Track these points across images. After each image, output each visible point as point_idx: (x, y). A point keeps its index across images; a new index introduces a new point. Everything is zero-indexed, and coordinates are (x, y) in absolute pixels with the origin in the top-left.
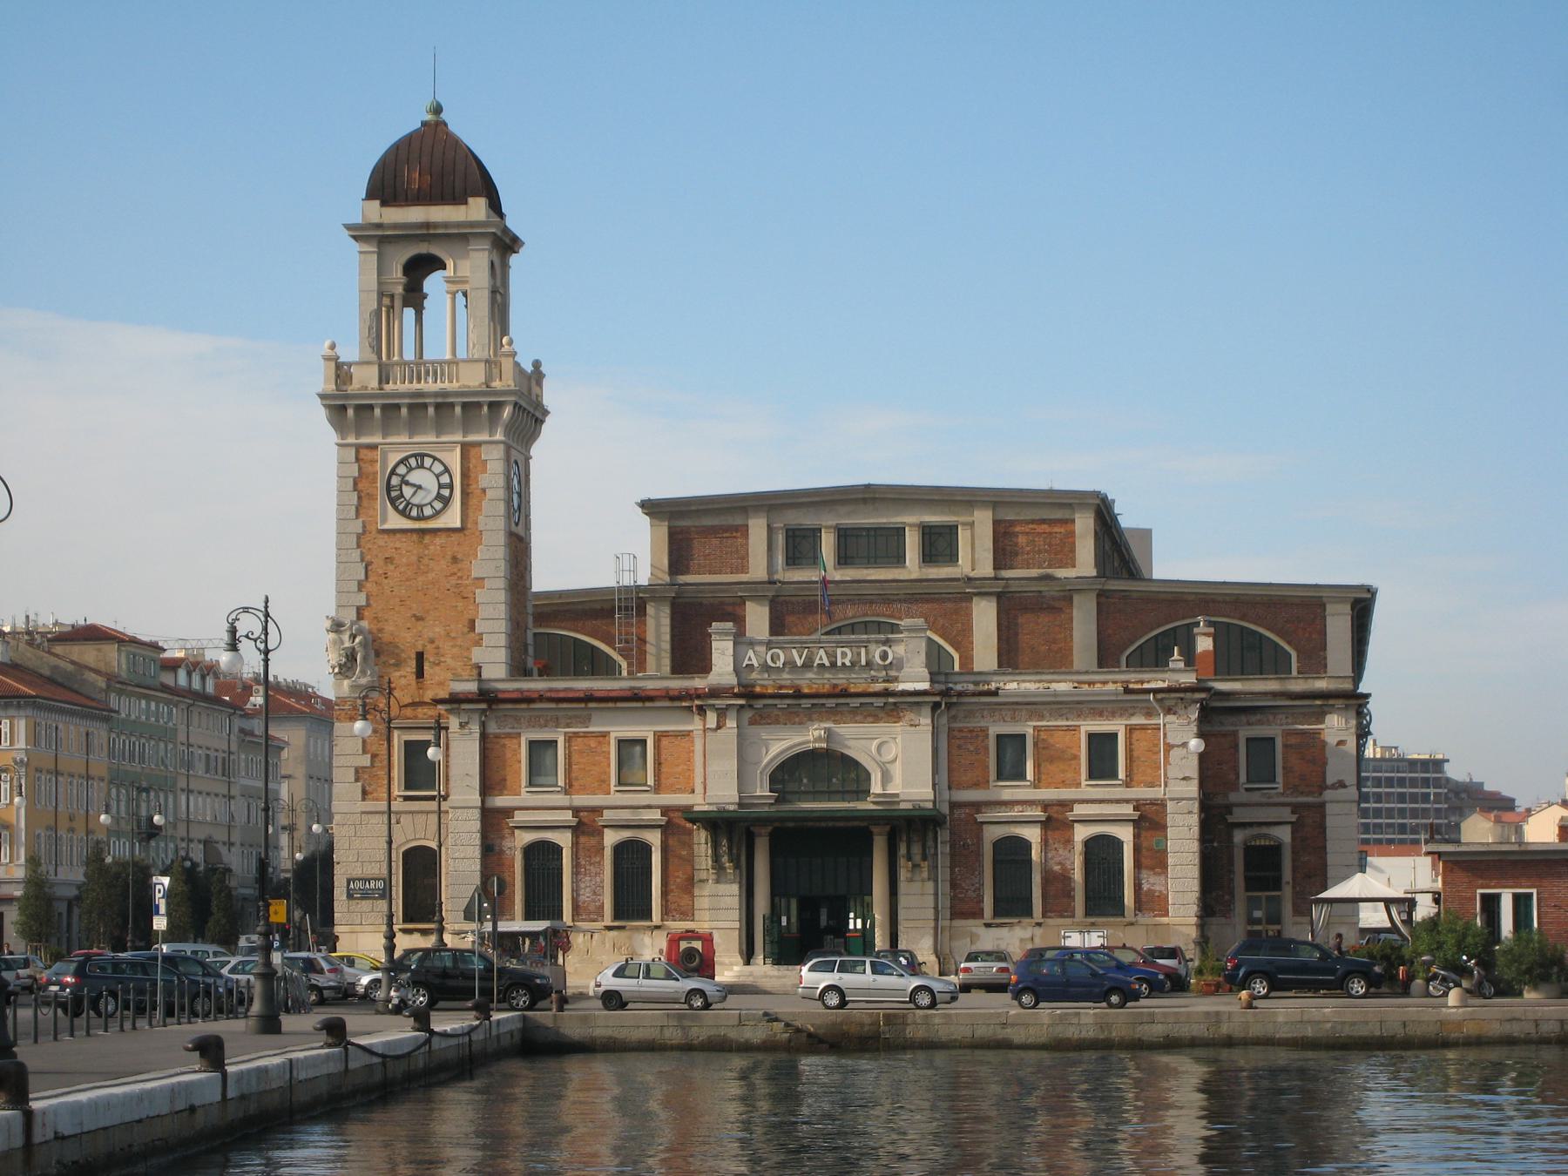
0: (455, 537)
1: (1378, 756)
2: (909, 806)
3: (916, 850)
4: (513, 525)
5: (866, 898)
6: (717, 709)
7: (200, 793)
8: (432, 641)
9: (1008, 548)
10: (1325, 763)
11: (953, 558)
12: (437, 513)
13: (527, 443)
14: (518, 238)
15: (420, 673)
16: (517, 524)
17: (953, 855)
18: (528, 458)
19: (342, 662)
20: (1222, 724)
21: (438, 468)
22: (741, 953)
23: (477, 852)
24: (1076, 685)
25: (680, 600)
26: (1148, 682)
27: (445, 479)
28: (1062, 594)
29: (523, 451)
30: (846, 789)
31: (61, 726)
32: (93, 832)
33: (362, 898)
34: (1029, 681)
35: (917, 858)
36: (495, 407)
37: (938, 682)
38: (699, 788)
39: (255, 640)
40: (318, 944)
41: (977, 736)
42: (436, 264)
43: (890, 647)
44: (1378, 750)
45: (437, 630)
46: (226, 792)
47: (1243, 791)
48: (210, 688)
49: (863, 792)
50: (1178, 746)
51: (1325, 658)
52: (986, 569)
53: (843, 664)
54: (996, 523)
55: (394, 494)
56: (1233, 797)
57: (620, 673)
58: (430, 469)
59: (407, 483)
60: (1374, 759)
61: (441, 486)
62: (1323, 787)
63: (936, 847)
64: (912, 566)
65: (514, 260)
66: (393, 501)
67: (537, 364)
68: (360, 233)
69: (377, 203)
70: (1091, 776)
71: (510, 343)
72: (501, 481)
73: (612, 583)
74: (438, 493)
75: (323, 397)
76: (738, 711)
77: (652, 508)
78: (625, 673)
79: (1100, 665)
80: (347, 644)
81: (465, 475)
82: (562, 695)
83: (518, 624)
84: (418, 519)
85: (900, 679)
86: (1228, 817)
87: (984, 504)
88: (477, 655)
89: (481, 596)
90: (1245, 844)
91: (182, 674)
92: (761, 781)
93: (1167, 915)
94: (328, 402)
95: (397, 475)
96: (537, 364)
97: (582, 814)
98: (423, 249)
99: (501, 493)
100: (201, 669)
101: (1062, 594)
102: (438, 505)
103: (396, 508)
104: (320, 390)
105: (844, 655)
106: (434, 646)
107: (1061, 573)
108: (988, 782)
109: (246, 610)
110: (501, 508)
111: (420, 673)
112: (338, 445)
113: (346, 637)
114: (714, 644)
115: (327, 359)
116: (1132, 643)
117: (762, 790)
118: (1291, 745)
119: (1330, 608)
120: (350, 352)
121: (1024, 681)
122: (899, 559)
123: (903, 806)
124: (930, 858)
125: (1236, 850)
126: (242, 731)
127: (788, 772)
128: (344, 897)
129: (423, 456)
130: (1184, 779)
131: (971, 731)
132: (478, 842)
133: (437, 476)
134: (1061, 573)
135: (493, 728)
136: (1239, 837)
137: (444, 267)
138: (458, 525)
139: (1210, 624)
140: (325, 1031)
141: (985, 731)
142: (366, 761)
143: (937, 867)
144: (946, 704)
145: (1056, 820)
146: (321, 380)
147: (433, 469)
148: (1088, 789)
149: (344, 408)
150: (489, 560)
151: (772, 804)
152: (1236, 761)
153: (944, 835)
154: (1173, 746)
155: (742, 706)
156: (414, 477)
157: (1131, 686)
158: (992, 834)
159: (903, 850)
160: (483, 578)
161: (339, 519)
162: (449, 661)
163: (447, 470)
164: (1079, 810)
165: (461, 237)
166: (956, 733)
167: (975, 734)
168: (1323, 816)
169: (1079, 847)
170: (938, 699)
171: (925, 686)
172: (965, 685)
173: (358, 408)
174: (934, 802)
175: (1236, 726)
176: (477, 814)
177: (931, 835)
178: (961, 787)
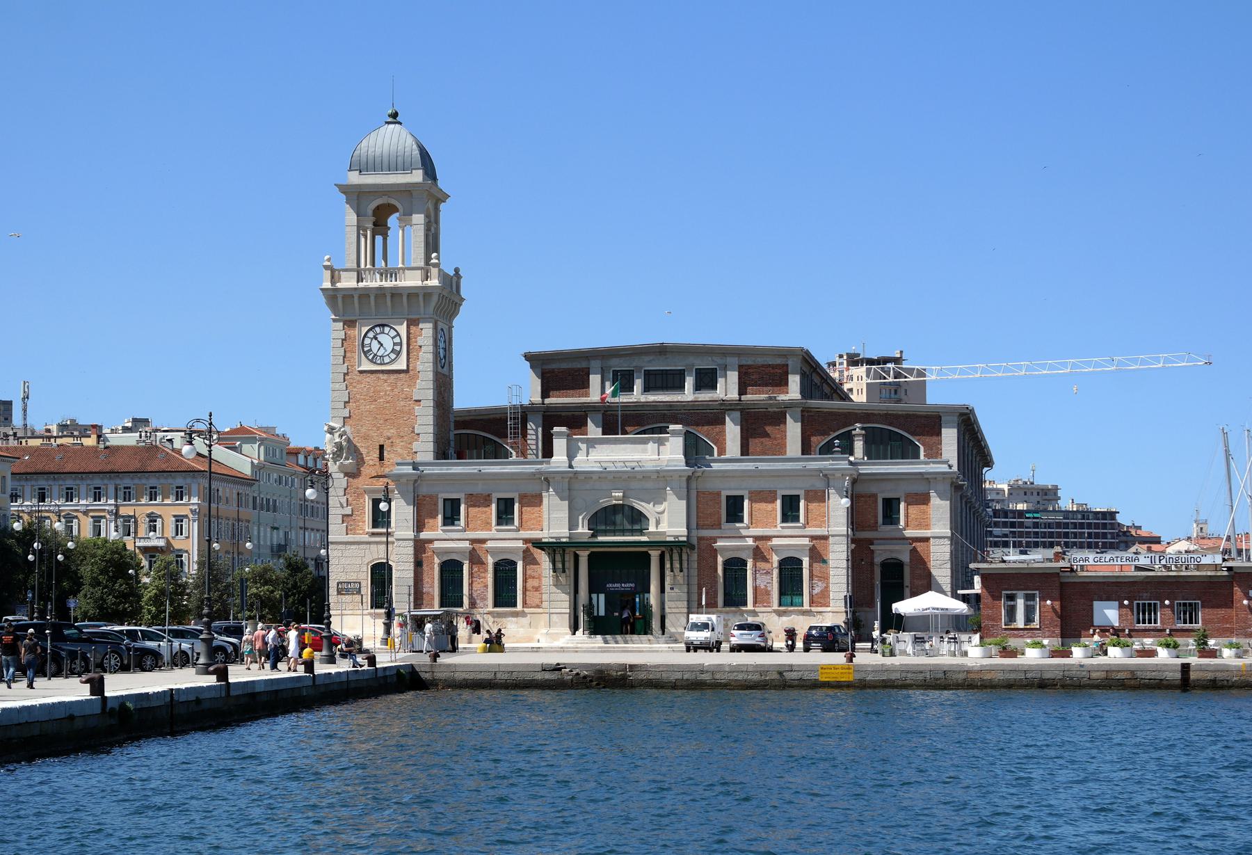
1: (1075, 509)
2: (672, 539)
4: (440, 367)
5: (646, 595)
7: (312, 530)
8: (389, 438)
12: (392, 361)
15: (381, 458)
16: (443, 368)
18: (450, 328)
21: (393, 333)
22: (570, 628)
27: (397, 340)
32: (242, 554)
35: (677, 571)
42: (392, 209)
44: (1075, 506)
45: (392, 431)
52: (733, 394)
55: (366, 349)
59: (376, 338)
60: (1073, 511)
61: (395, 344)
65: (442, 206)
66: (365, 353)
67: (457, 270)
71: (438, 258)
72: (431, 341)
77: (529, 357)
80: (337, 440)
88: (416, 446)
89: (418, 409)
96: (457, 270)
99: (431, 348)
102: (393, 356)
103: (367, 357)
109: (198, 420)
110: (430, 357)
111: (381, 458)
113: (337, 435)
117: (583, 530)
123: (668, 539)
128: (336, 593)
133: (393, 338)
137: (396, 210)
138: (405, 367)
140: (88, 686)
142: (348, 511)
150: (424, 388)
156: (381, 338)
158: (878, 560)
159: (668, 565)
160: (420, 401)
162: (399, 450)
163: (398, 334)
165: (406, 191)
169: (776, 564)
173: (344, 297)
174: (688, 537)
176: (411, 543)
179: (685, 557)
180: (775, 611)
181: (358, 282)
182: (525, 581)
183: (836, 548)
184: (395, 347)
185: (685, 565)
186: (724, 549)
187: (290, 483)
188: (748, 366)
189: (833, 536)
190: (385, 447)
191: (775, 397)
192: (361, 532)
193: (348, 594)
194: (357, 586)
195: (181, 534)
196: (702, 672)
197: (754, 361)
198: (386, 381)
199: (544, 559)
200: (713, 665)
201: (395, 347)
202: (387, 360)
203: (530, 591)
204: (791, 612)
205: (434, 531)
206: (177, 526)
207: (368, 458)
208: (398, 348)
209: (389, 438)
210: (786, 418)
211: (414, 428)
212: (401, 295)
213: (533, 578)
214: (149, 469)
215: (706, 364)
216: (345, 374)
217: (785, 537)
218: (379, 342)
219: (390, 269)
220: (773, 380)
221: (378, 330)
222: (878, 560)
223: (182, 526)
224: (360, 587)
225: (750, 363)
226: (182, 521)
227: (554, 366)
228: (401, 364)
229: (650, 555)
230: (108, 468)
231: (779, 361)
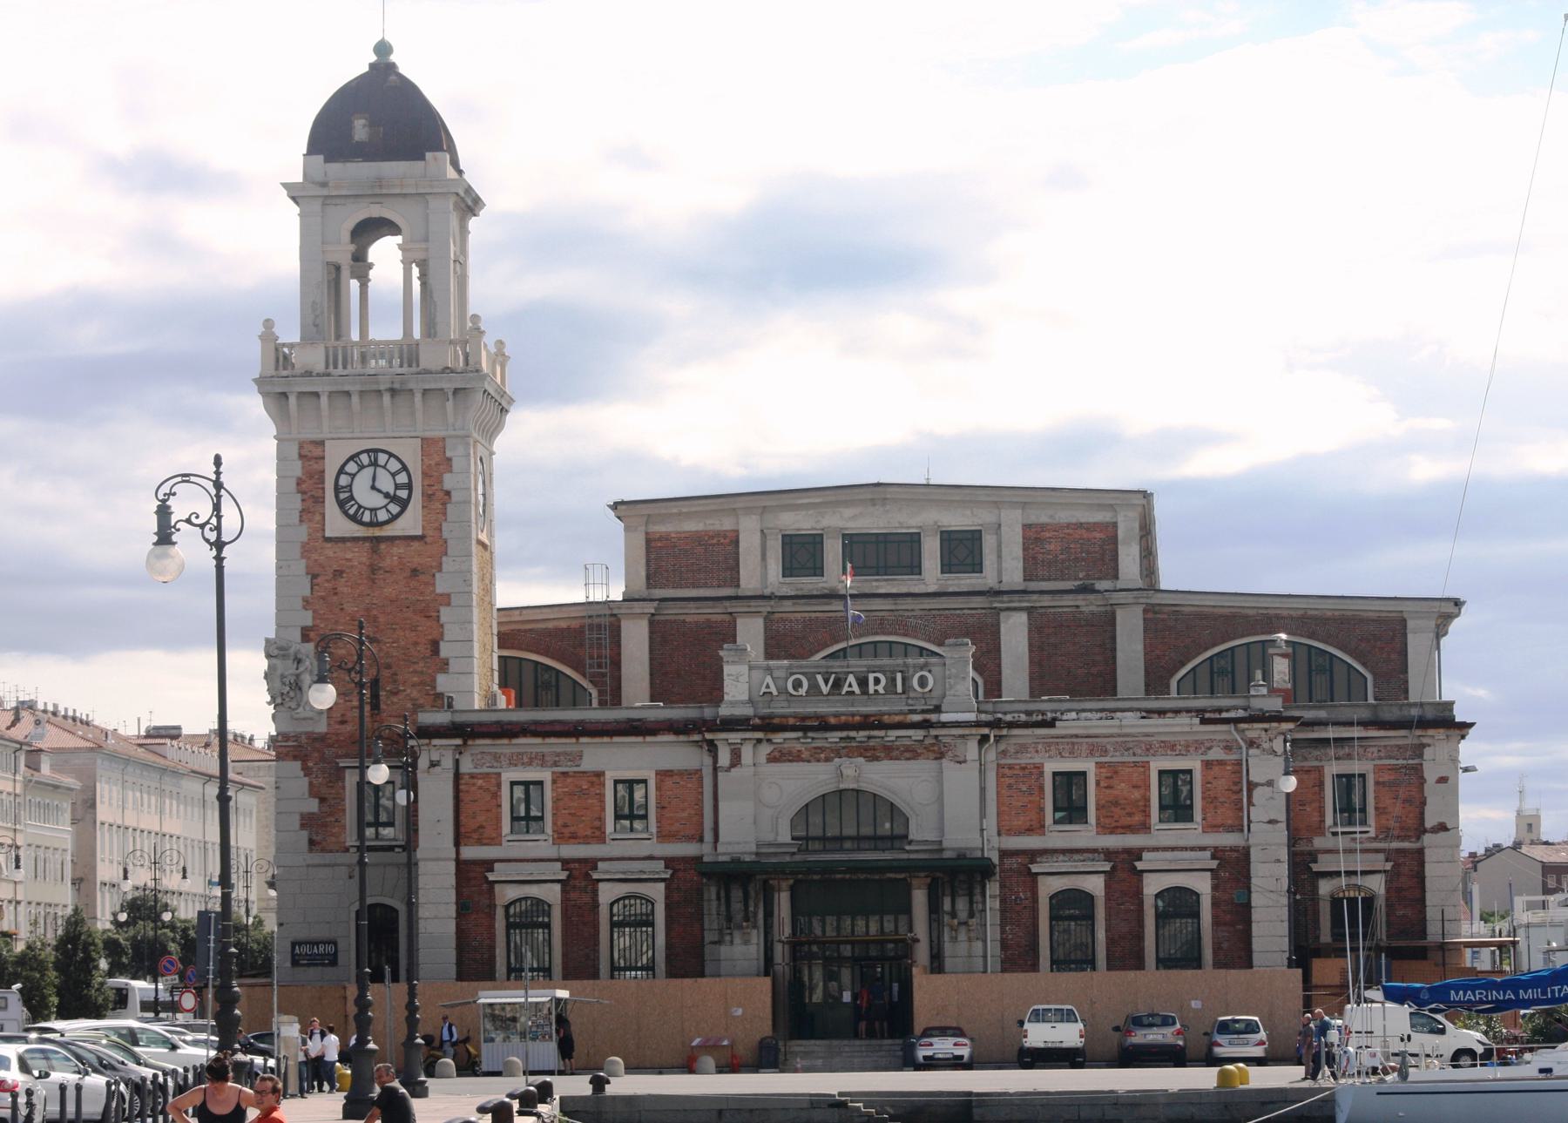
0: (416, 545)
3: (962, 905)
6: (729, 744)
9: (1040, 557)
10: (1424, 803)
11: (977, 567)
13: (491, 436)
14: (480, 199)
17: (1003, 911)
20: (1306, 759)
21: (394, 465)
23: (452, 910)
24: (1144, 714)
25: (662, 618)
26: (1227, 711)
29: (487, 445)
33: (308, 965)
34: (1090, 711)
37: (986, 712)
38: (708, 836)
39: (349, 671)
41: (1031, 773)
43: (930, 671)
47: (1330, 835)
50: (1262, 785)
51: (1407, 682)
52: (1014, 575)
53: (876, 691)
54: (1026, 527)
56: (1318, 843)
57: (591, 704)
58: (384, 467)
62: (1421, 830)
63: (984, 902)
64: (932, 575)
65: (473, 223)
66: (341, 504)
69: (321, 158)
76: (755, 745)
78: (595, 703)
79: (1147, 692)
82: (548, 728)
83: (485, 646)
84: (371, 524)
85: (943, 709)
86: (1312, 865)
90: (1332, 896)
94: (269, 388)
95: (347, 473)
97: (572, 866)
98: (375, 211)
101: (1102, 609)
102: (395, 509)
103: (346, 513)
105: (877, 681)
108: (1043, 826)
114: (727, 669)
116: (1183, 664)
118: (1383, 783)
119: (1411, 624)
121: (1084, 711)
122: (915, 568)
123: (947, 855)
124: (977, 915)
125: (1321, 903)
129: (376, 451)
130: (1270, 822)
131: (1023, 769)
133: (393, 475)
135: (467, 766)
136: (1325, 887)
139: (1280, 647)
141: (1039, 769)
142: (313, 806)
143: (985, 925)
144: (995, 736)
147: (388, 467)
149: (284, 395)
151: (794, 854)
152: (1322, 799)
153: (993, 888)
154: (1257, 785)
155: (759, 741)
157: (1207, 715)
158: (1049, 887)
163: (405, 468)
166: (1006, 771)
167: (1027, 772)
168: (1422, 864)
170: (986, 731)
171: (971, 717)
172: (1016, 715)
175: (1321, 760)
176: (452, 866)
177: (978, 890)
178: (1012, 832)
194: (330, 949)
197: (1051, 517)
215: (958, 520)
218: (379, 491)
220: (1088, 553)
225: (1044, 519)
228: (410, 522)
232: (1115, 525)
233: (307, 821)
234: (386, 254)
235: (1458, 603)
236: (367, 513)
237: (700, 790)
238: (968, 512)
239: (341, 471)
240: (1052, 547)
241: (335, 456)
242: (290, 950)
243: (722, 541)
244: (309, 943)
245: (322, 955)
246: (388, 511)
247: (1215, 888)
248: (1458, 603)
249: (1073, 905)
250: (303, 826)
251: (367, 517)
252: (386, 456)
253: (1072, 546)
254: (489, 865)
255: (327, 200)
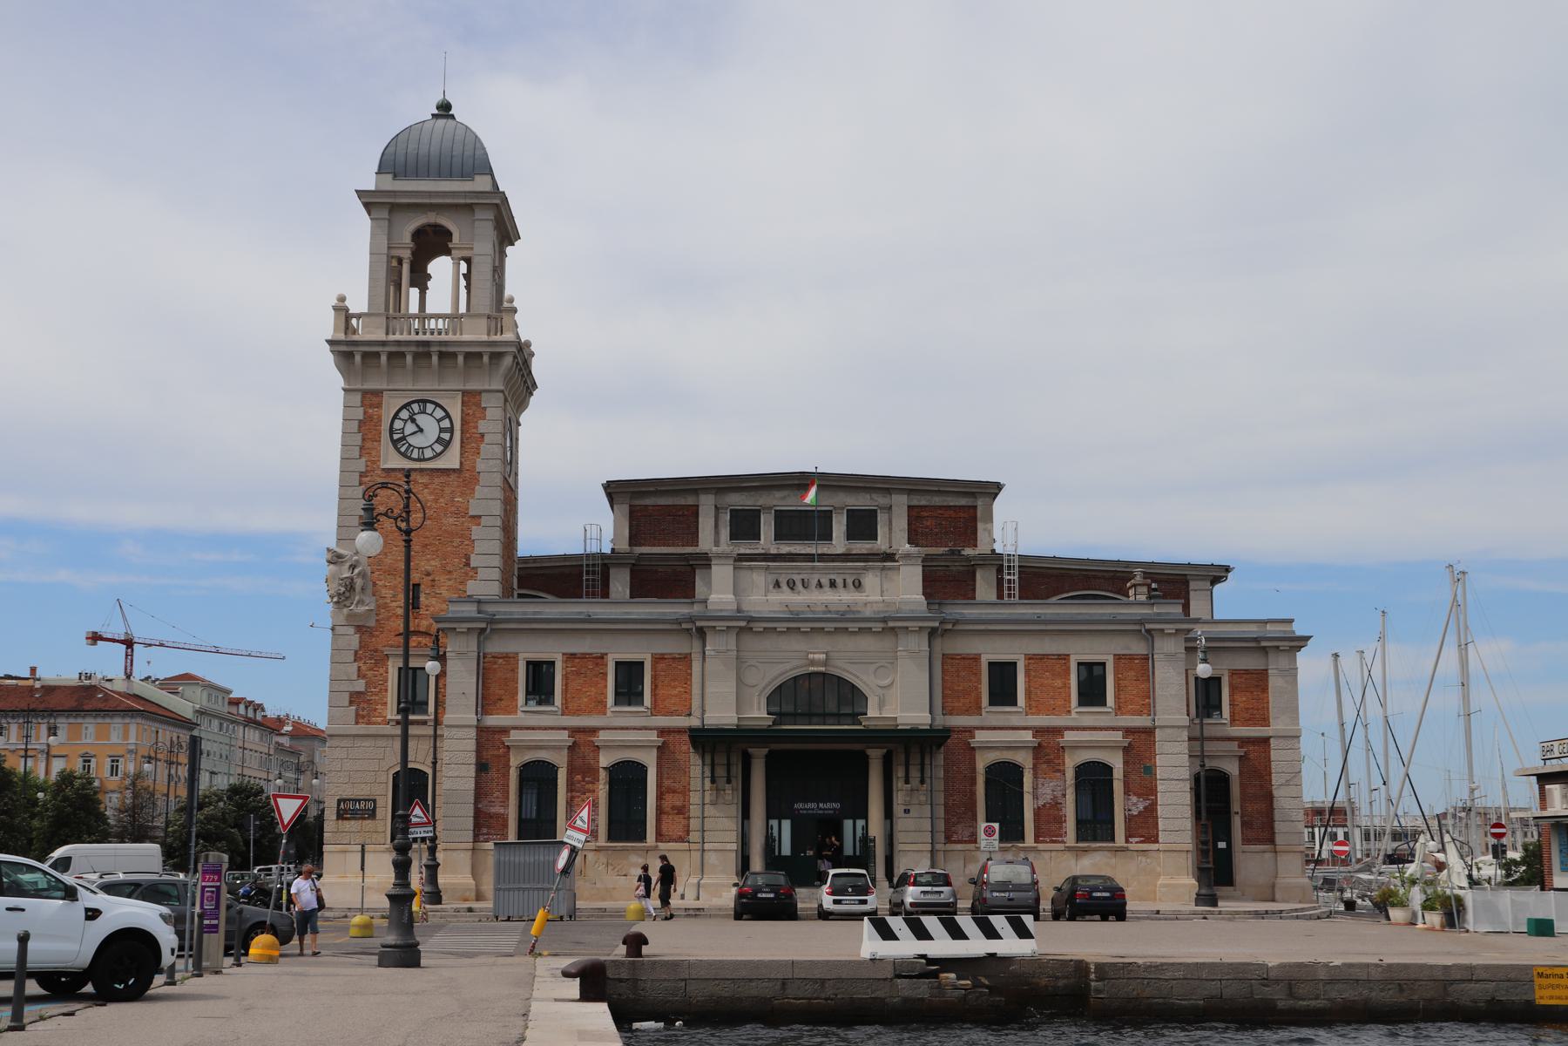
3: (915, 773)
8: (428, 574)
9: (920, 530)
11: (873, 536)
19: (341, 592)
21: (439, 413)
27: (446, 424)
28: (966, 568)
30: (842, 712)
31: (160, 731)
35: (915, 782)
36: (496, 357)
40: (1449, 898)
45: (433, 563)
46: (266, 777)
48: (259, 718)
49: (855, 717)
54: (910, 508)
59: (413, 421)
61: (442, 430)
66: (395, 443)
68: (370, 201)
70: (1081, 704)
73: (577, 549)
74: (439, 437)
75: (330, 342)
81: (464, 422)
87: (901, 491)
89: (476, 532)
91: (242, 707)
92: (759, 703)
93: (1156, 841)
100: (254, 706)
101: (966, 568)
102: (438, 448)
103: (398, 450)
104: (330, 338)
106: (430, 578)
107: (968, 551)
108: (980, 708)
112: (344, 390)
115: (336, 309)
119: (1193, 585)
120: (359, 303)
122: (827, 536)
126: (277, 743)
127: (787, 695)
128: (335, 818)
129: (425, 402)
132: (473, 760)
133: (439, 421)
134: (968, 551)
141: (976, 659)
142: (360, 686)
145: (1047, 748)
146: (327, 327)
148: (1079, 714)
155: (741, 628)
156: (420, 419)
158: (982, 762)
160: (480, 517)
161: (341, 471)
163: (448, 416)
164: (1069, 736)
165: (465, 207)
169: (1070, 774)
173: (365, 355)
176: (473, 733)
179: (927, 761)
180: (1069, 849)
181: (387, 334)
182: (660, 797)
183: (1168, 747)
184: (443, 435)
185: (927, 773)
186: (1077, 746)
187: (225, 729)
188: (921, 506)
189: (1161, 727)
190: (422, 587)
191: (959, 551)
192: (379, 719)
193: (355, 819)
194: (370, 805)
195: (117, 775)
196: (1266, 981)
198: (426, 486)
199: (696, 768)
200: (1291, 966)
201: (443, 435)
202: (428, 453)
203: (668, 814)
204: (1095, 850)
205: (509, 713)
206: (112, 766)
207: (394, 604)
208: (446, 436)
209: (428, 574)
210: (974, 580)
211: (468, 558)
212: (454, 355)
213: (674, 792)
214: (86, 708)
215: (861, 502)
216: (362, 475)
217: (1084, 729)
219: (161, 868)
221: (415, 407)
222: (982, 762)
223: (117, 766)
224: (375, 807)
226: (118, 761)
227: (649, 501)
228: (451, 460)
229: (868, 756)
230: (42, 707)
231: (963, 502)
232: (975, 507)
233: (355, 697)
234: (441, 269)
235: (1227, 569)
236: (416, 451)
237: (689, 671)
238: (868, 496)
239: (396, 416)
240: (929, 523)
241: (391, 405)
242: (336, 805)
243: (686, 513)
244: (353, 800)
245: (362, 810)
246: (433, 449)
247: (1126, 763)
248: (1227, 569)
249: (1005, 779)
250: (351, 703)
251: (415, 455)
252: (438, 451)
253: (943, 523)
254: (505, 731)
255: (394, 208)
